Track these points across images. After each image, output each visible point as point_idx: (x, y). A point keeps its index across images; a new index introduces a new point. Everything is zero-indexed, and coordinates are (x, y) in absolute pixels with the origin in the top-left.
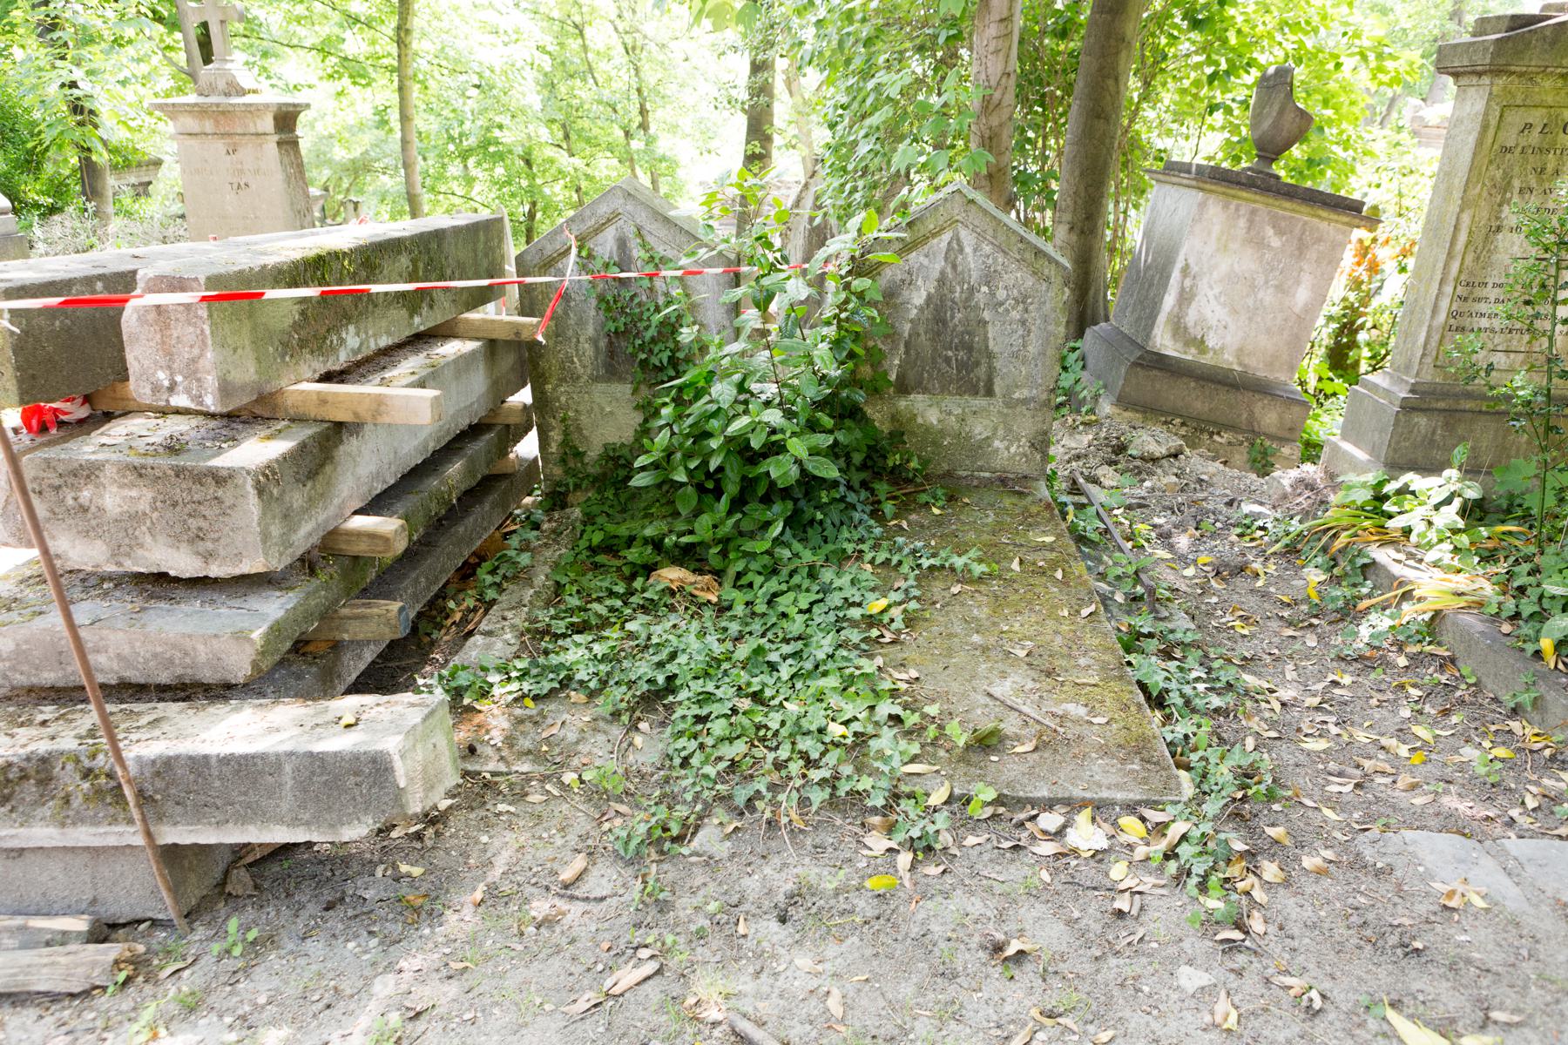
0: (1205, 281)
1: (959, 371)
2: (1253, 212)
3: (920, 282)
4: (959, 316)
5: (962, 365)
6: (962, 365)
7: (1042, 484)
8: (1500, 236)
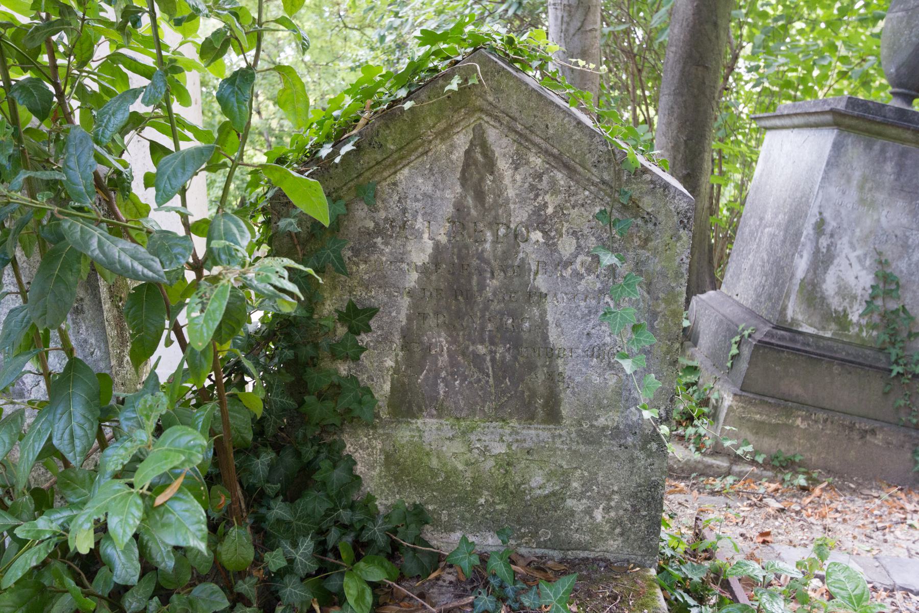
0: (845, 240)
1: (498, 380)
2: (903, 154)
4: (493, 284)
5: (503, 370)
6: (503, 370)
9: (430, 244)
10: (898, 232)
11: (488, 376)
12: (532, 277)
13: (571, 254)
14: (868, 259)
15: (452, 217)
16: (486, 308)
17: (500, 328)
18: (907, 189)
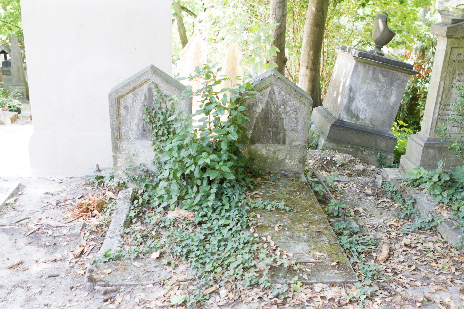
0: (358, 94)
1: (273, 136)
2: (375, 69)
3: (259, 104)
5: (274, 133)
6: (274, 133)
7: (303, 175)
8: (453, 89)
16: (272, 121)
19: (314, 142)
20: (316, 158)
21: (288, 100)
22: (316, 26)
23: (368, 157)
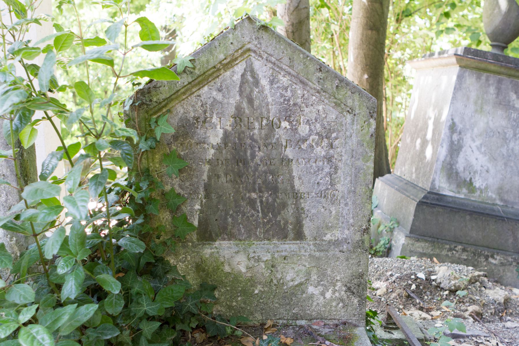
0: (469, 135)
1: (265, 215)
2: (500, 82)
3: (215, 120)
4: (260, 154)
9: (221, 131)
10: (499, 130)
11: (258, 212)
12: (283, 149)
13: (306, 135)
14: (483, 147)
15: (235, 115)
16: (256, 170)
17: (265, 182)
18: (503, 103)
19: (382, 242)
20: (391, 275)
21: (299, 101)
22: (371, 29)
23: (501, 269)
